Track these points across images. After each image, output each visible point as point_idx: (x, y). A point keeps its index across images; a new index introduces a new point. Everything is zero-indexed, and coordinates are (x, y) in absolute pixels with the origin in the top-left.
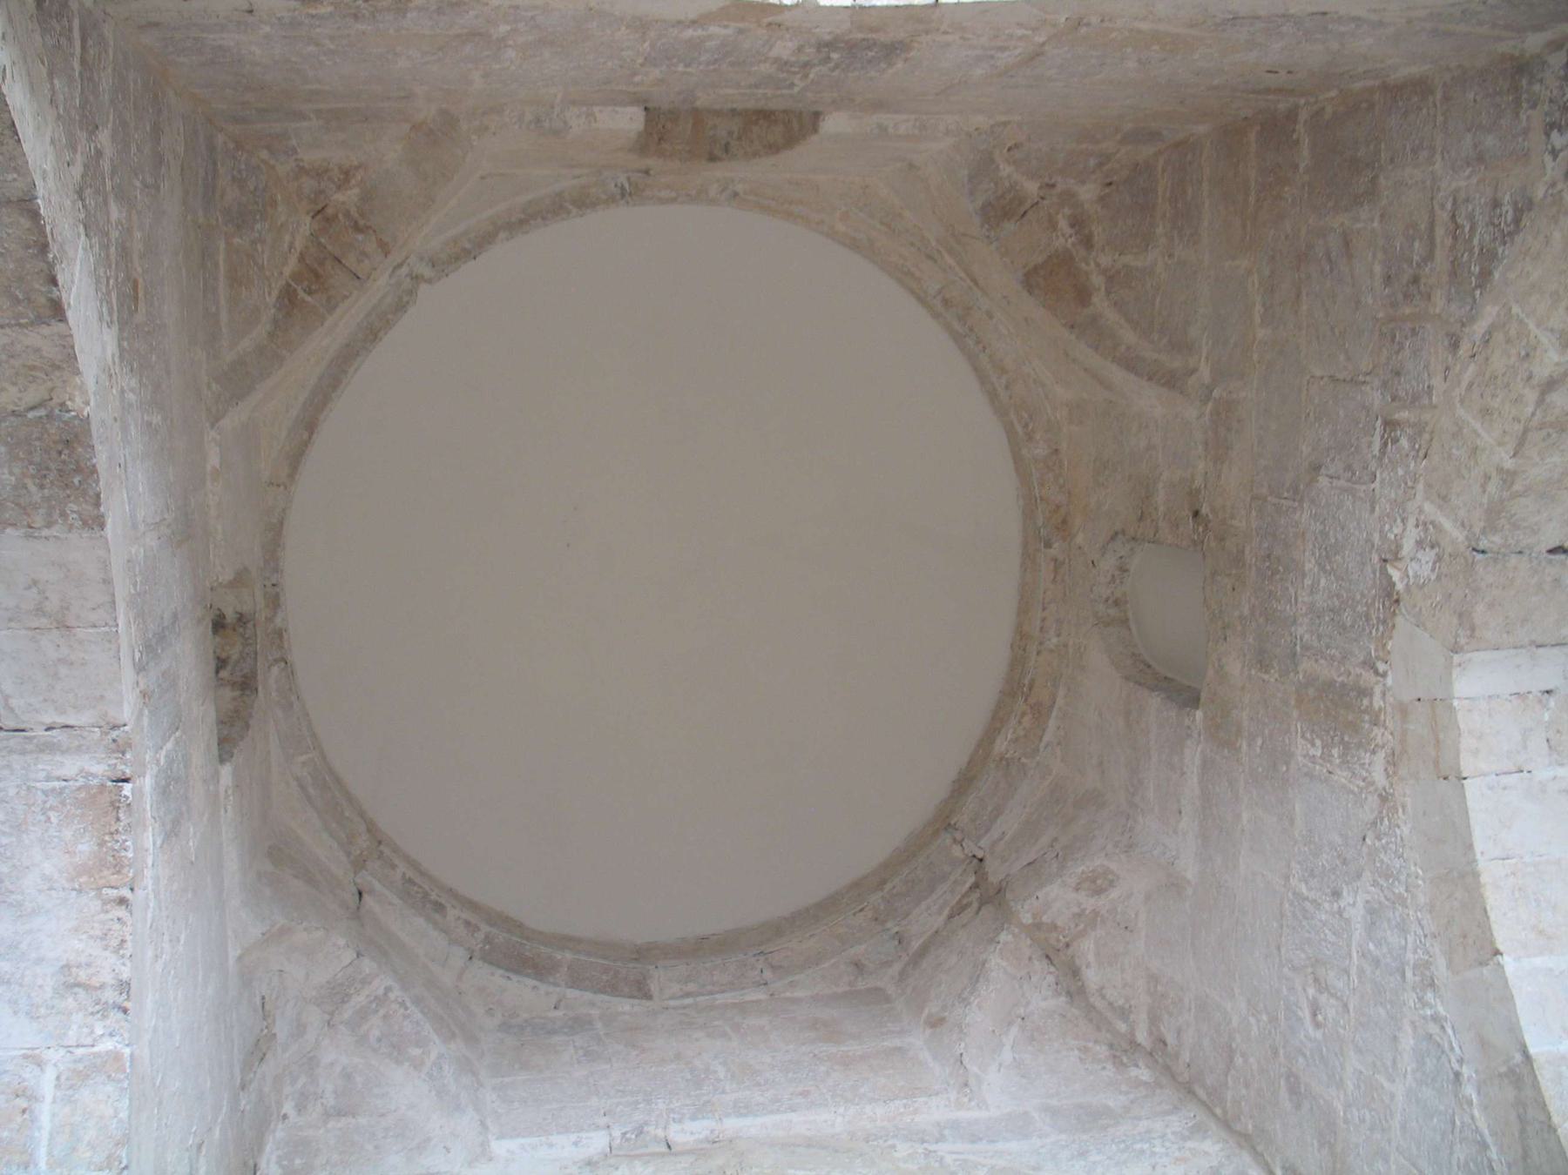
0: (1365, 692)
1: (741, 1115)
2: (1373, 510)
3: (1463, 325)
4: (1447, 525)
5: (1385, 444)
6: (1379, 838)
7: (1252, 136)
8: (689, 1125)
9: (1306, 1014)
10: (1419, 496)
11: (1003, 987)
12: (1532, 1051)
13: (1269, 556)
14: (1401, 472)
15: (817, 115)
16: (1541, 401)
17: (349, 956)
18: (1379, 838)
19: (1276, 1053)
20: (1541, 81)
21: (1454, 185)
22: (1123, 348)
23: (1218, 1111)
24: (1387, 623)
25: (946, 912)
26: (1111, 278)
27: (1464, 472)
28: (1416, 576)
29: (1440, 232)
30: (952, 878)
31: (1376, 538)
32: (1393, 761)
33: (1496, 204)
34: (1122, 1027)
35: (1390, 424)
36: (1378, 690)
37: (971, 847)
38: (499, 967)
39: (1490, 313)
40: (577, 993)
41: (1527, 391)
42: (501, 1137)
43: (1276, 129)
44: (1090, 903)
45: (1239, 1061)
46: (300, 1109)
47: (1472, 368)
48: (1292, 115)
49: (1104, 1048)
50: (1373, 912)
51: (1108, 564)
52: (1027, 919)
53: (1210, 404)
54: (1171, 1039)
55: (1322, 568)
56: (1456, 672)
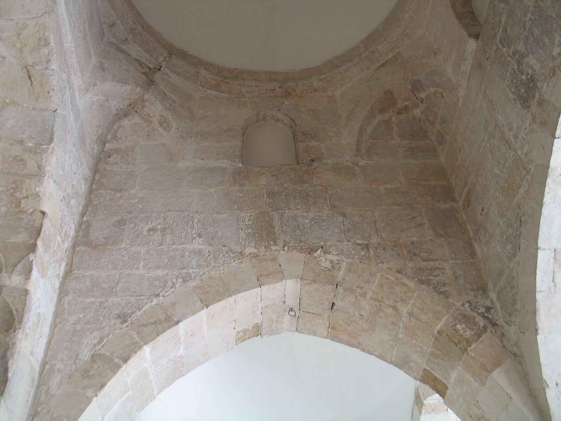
0: (275, 243)
2: (338, 241)
3: (406, 275)
4: (342, 273)
5: (360, 245)
6: (227, 253)
7: (444, 182)
9: (150, 226)
10: (347, 260)
11: (118, 92)
12: (180, 324)
13: (308, 195)
14: (353, 252)
15: (476, 37)
16: (390, 306)
18: (227, 253)
19: (130, 213)
20: (482, 298)
21: (447, 268)
22: (365, 128)
23: (94, 186)
24: (301, 250)
25: (138, 58)
26: (388, 122)
27: (361, 278)
28: (321, 261)
29: (432, 263)
30: (152, 59)
31: (329, 243)
32: (255, 256)
33: (444, 285)
34: (109, 137)
35: (367, 247)
36: (277, 248)
37: (164, 64)
39: (412, 284)
41: (392, 301)
43: (448, 193)
44: (155, 120)
45: (118, 195)
47: (393, 279)
48: (454, 200)
50: (200, 252)
51: (280, 116)
52: (146, 97)
53: (352, 165)
54: (112, 160)
55: (312, 219)
56: (295, 280)
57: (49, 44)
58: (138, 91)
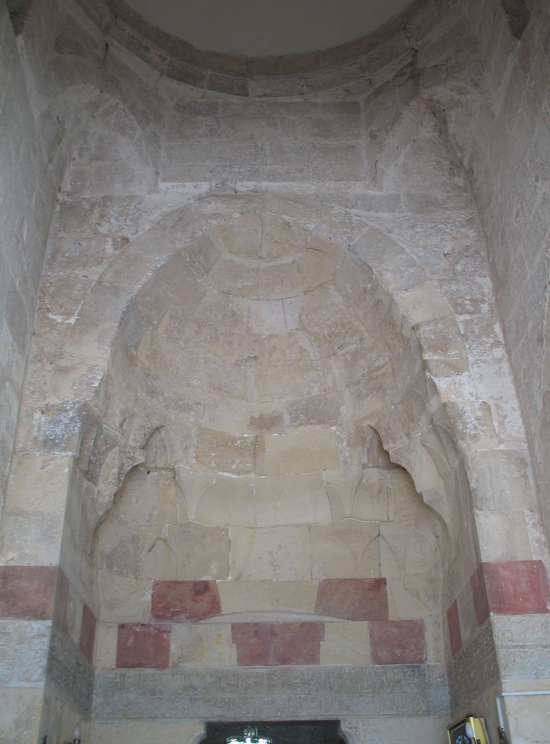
1: (271, 180)
8: (246, 183)
9: (515, 213)
17: (97, 92)
23: (481, 216)
25: (395, 73)
30: (401, 57)
34: (459, 155)
38: (175, 79)
40: (211, 92)
42: (164, 180)
44: (457, 97)
46: (80, 155)
49: (448, 163)
52: (425, 97)
57: (288, 222)
58: (416, 104)
